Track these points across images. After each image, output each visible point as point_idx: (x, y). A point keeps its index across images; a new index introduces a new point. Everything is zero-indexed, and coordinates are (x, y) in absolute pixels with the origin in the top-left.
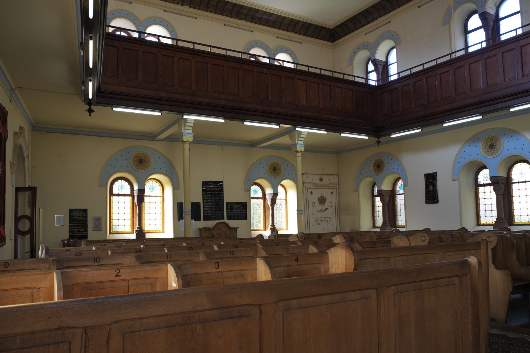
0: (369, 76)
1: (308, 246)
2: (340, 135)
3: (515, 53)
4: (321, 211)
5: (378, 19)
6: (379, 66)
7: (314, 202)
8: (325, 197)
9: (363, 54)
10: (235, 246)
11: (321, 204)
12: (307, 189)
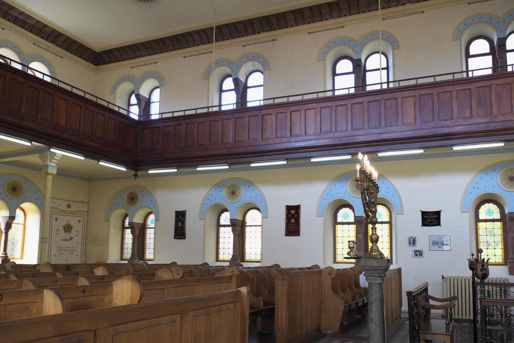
0: (131, 109)
1: (78, 278)
2: (99, 163)
3: (258, 119)
4: (66, 240)
5: (145, 57)
6: (142, 101)
7: (58, 230)
8: (71, 225)
9: (127, 87)
10: (34, 275)
11: (66, 233)
12: (51, 215)
